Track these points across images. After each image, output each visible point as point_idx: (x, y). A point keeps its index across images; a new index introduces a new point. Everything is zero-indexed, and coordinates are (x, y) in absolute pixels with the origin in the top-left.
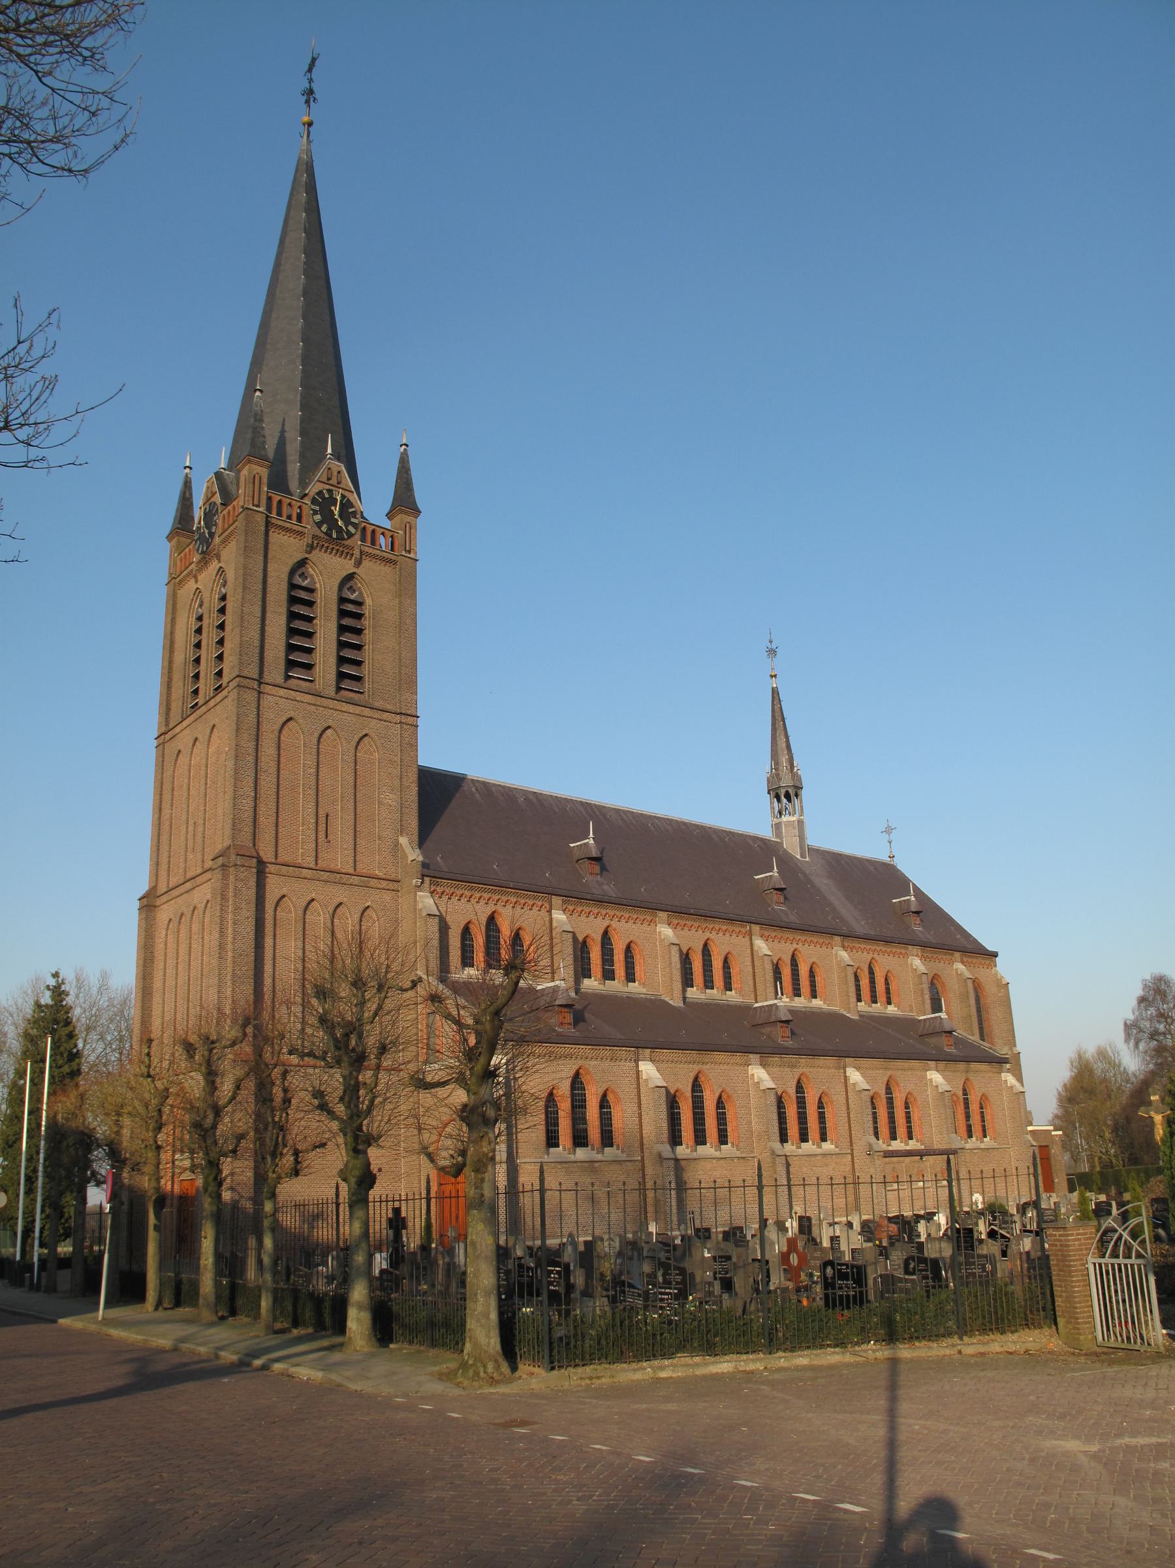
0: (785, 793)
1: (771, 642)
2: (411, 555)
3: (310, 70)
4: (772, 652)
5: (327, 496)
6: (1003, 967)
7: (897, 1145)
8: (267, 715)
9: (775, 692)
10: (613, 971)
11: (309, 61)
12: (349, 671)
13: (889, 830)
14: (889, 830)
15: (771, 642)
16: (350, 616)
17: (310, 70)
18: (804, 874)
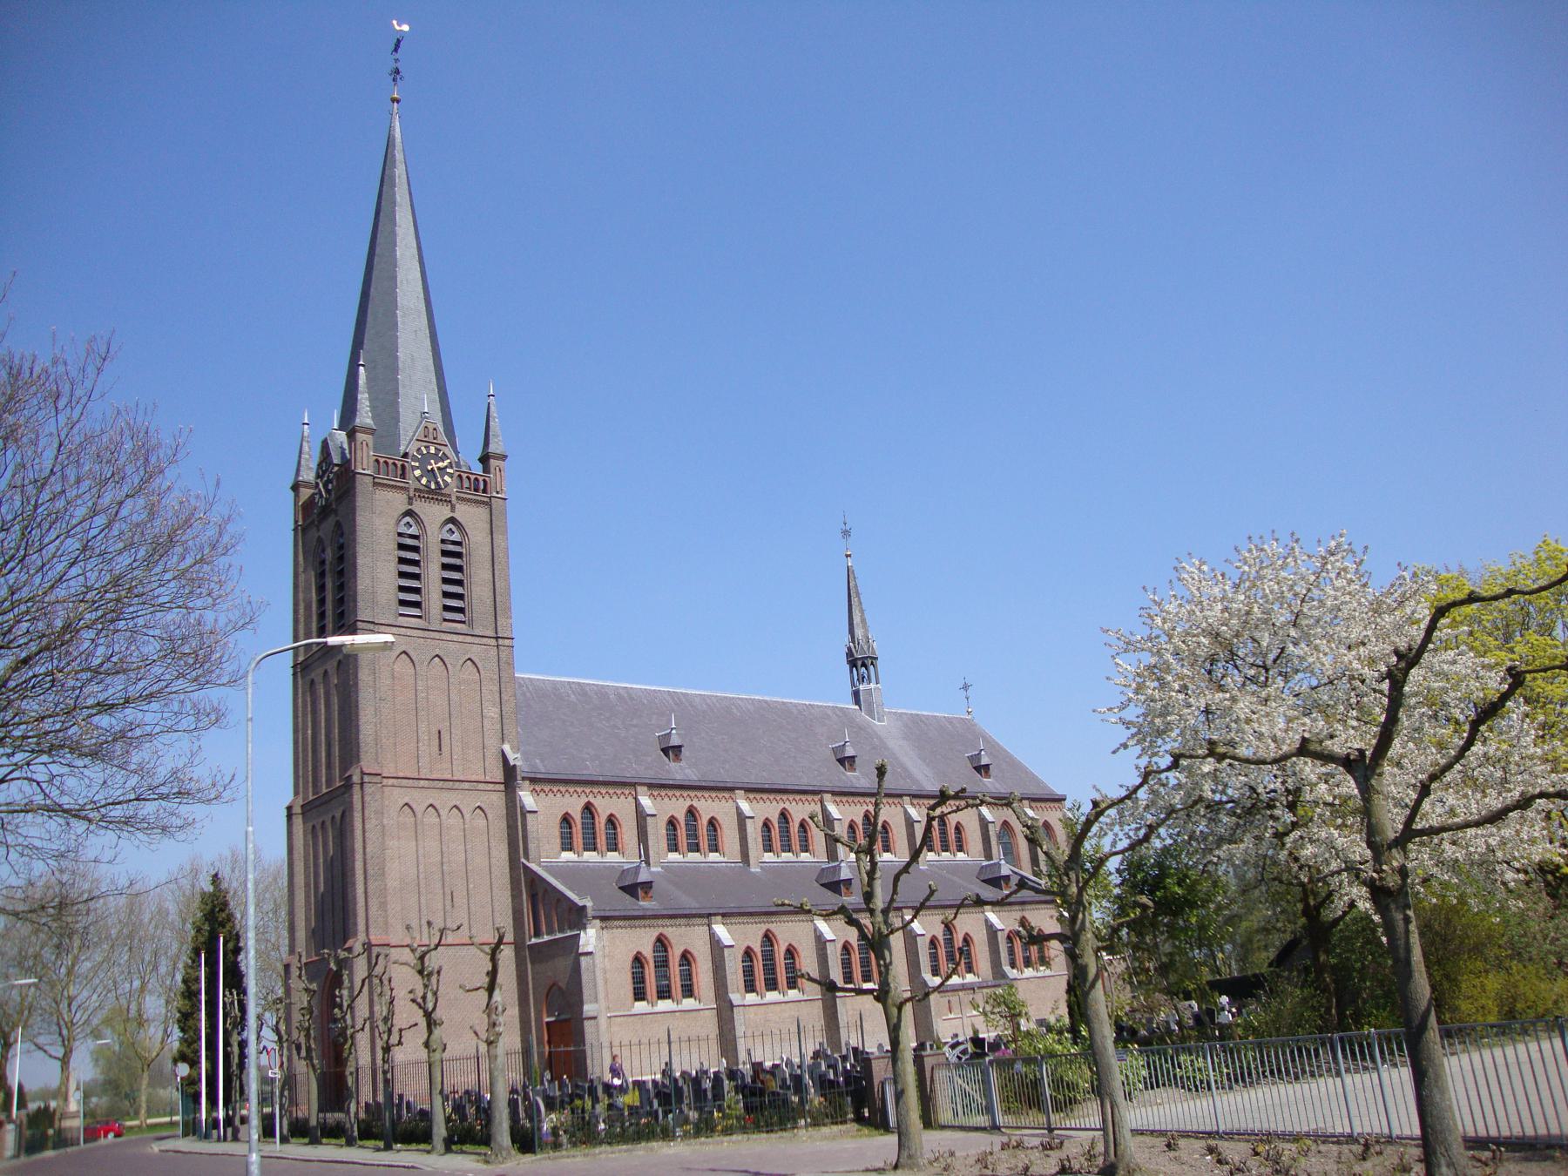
3: (396, 50)
10: (697, 845)
12: (456, 603)
13: (966, 687)
14: (966, 687)
16: (454, 559)
17: (396, 50)
18: (879, 738)
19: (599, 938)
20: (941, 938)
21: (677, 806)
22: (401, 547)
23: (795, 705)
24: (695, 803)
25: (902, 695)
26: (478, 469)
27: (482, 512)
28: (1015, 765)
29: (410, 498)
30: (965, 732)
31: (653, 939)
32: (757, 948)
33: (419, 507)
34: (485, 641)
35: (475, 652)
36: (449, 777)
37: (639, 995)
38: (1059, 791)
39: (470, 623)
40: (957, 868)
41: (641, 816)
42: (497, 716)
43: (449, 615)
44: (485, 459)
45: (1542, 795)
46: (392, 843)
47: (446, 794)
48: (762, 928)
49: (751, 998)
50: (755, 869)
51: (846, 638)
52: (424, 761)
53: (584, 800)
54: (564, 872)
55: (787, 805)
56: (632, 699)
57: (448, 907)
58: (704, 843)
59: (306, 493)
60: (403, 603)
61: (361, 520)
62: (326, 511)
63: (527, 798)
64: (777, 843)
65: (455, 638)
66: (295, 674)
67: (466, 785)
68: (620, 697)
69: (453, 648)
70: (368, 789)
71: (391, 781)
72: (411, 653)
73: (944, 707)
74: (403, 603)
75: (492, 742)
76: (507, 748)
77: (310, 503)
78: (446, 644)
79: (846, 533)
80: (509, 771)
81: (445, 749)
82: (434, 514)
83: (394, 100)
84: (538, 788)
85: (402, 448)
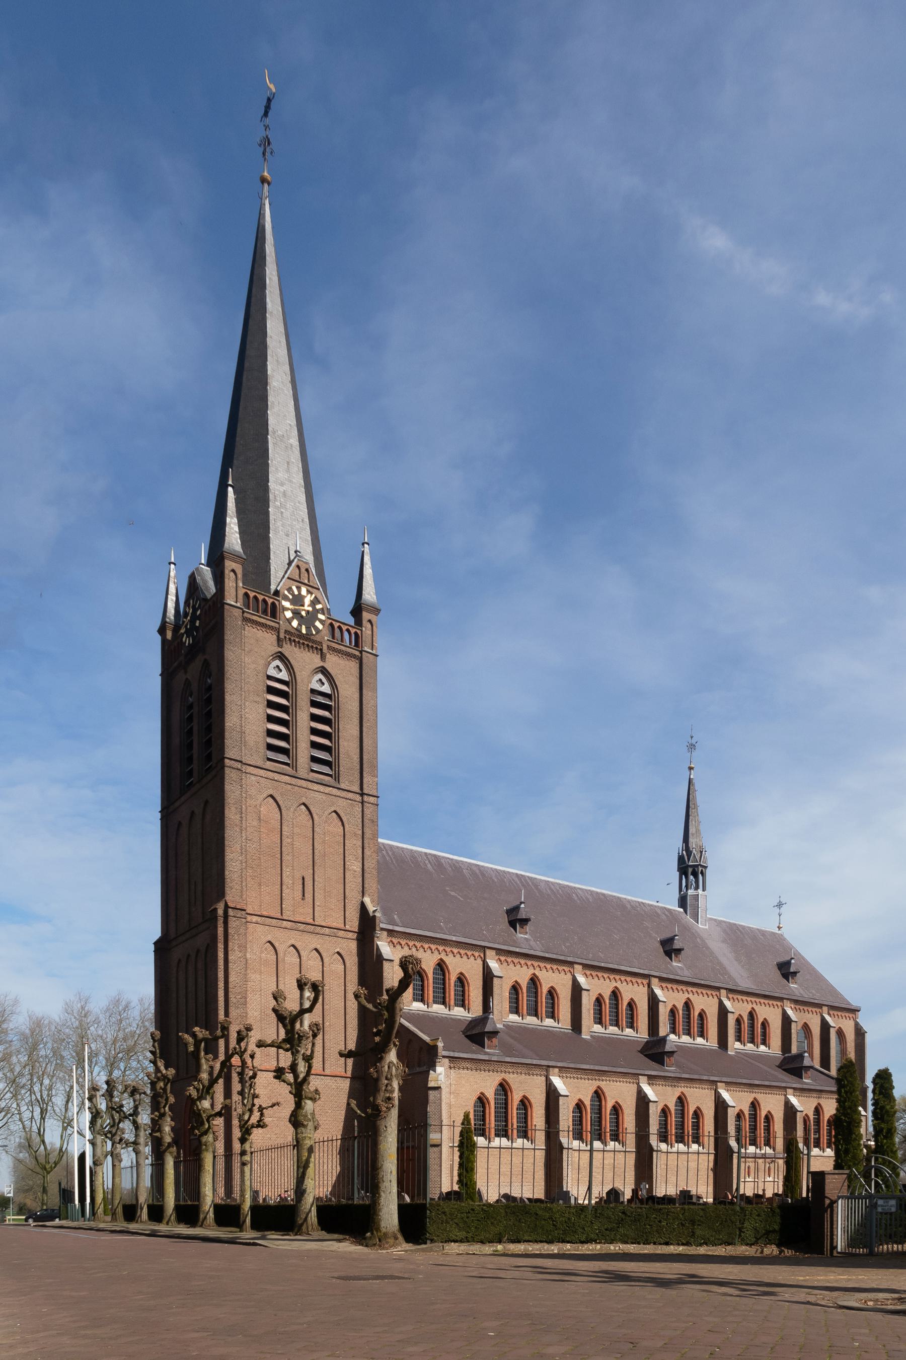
0: (690, 869)
2: (374, 652)
3: (266, 114)
5: (296, 593)
8: (305, 776)
11: (264, 103)
12: (326, 755)
13: (780, 905)
14: (780, 905)
16: (325, 706)
17: (266, 114)
18: (701, 938)
19: (447, 1076)
20: (747, 1113)
21: (521, 974)
22: (271, 690)
23: (629, 901)
24: (537, 972)
25: (718, 903)
28: (817, 977)
30: (775, 941)
31: (497, 1083)
32: (672, 1108)
33: (289, 650)
34: (350, 795)
35: (341, 805)
38: (854, 1003)
39: (337, 778)
40: (760, 1057)
41: (488, 978)
42: (360, 870)
43: (316, 767)
44: (357, 611)
46: (253, 976)
47: (307, 937)
50: (585, 1036)
51: (679, 843)
54: (415, 1018)
55: (618, 985)
56: (483, 874)
60: (270, 747)
61: (230, 654)
62: (194, 651)
63: (384, 947)
64: (607, 1017)
65: (322, 788)
68: (473, 873)
69: (318, 796)
71: (255, 919)
73: (759, 919)
74: (270, 747)
76: (367, 900)
78: (312, 794)
79: (692, 747)
81: (309, 896)
83: (263, 180)
84: (395, 941)
85: (273, 588)
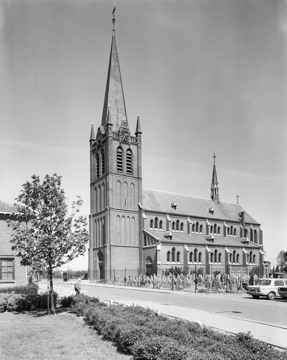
1: (214, 154)
3: (113, 13)
4: (214, 157)
6: (261, 227)
7: (234, 264)
9: (214, 166)
10: (178, 228)
12: (130, 171)
13: (238, 197)
14: (238, 197)
15: (214, 154)
16: (129, 159)
17: (113, 13)
19: (161, 247)
24: (179, 219)
26: (135, 136)
27: (135, 147)
29: (120, 143)
33: (122, 145)
36: (127, 210)
37: (168, 260)
38: (259, 223)
39: (133, 175)
43: (128, 173)
44: (136, 134)
45: (56, 267)
48: (195, 248)
49: (191, 263)
52: (122, 206)
53: (156, 217)
57: (126, 239)
58: (180, 228)
59: (93, 142)
63: (144, 215)
66: (91, 186)
67: (131, 212)
69: (130, 180)
70: (111, 211)
72: (134, 183)
75: (136, 202)
77: (95, 144)
78: (127, 179)
80: (140, 209)
82: (125, 147)
